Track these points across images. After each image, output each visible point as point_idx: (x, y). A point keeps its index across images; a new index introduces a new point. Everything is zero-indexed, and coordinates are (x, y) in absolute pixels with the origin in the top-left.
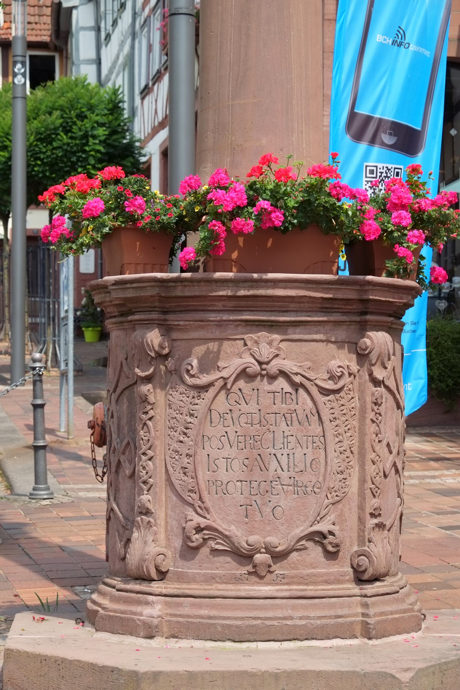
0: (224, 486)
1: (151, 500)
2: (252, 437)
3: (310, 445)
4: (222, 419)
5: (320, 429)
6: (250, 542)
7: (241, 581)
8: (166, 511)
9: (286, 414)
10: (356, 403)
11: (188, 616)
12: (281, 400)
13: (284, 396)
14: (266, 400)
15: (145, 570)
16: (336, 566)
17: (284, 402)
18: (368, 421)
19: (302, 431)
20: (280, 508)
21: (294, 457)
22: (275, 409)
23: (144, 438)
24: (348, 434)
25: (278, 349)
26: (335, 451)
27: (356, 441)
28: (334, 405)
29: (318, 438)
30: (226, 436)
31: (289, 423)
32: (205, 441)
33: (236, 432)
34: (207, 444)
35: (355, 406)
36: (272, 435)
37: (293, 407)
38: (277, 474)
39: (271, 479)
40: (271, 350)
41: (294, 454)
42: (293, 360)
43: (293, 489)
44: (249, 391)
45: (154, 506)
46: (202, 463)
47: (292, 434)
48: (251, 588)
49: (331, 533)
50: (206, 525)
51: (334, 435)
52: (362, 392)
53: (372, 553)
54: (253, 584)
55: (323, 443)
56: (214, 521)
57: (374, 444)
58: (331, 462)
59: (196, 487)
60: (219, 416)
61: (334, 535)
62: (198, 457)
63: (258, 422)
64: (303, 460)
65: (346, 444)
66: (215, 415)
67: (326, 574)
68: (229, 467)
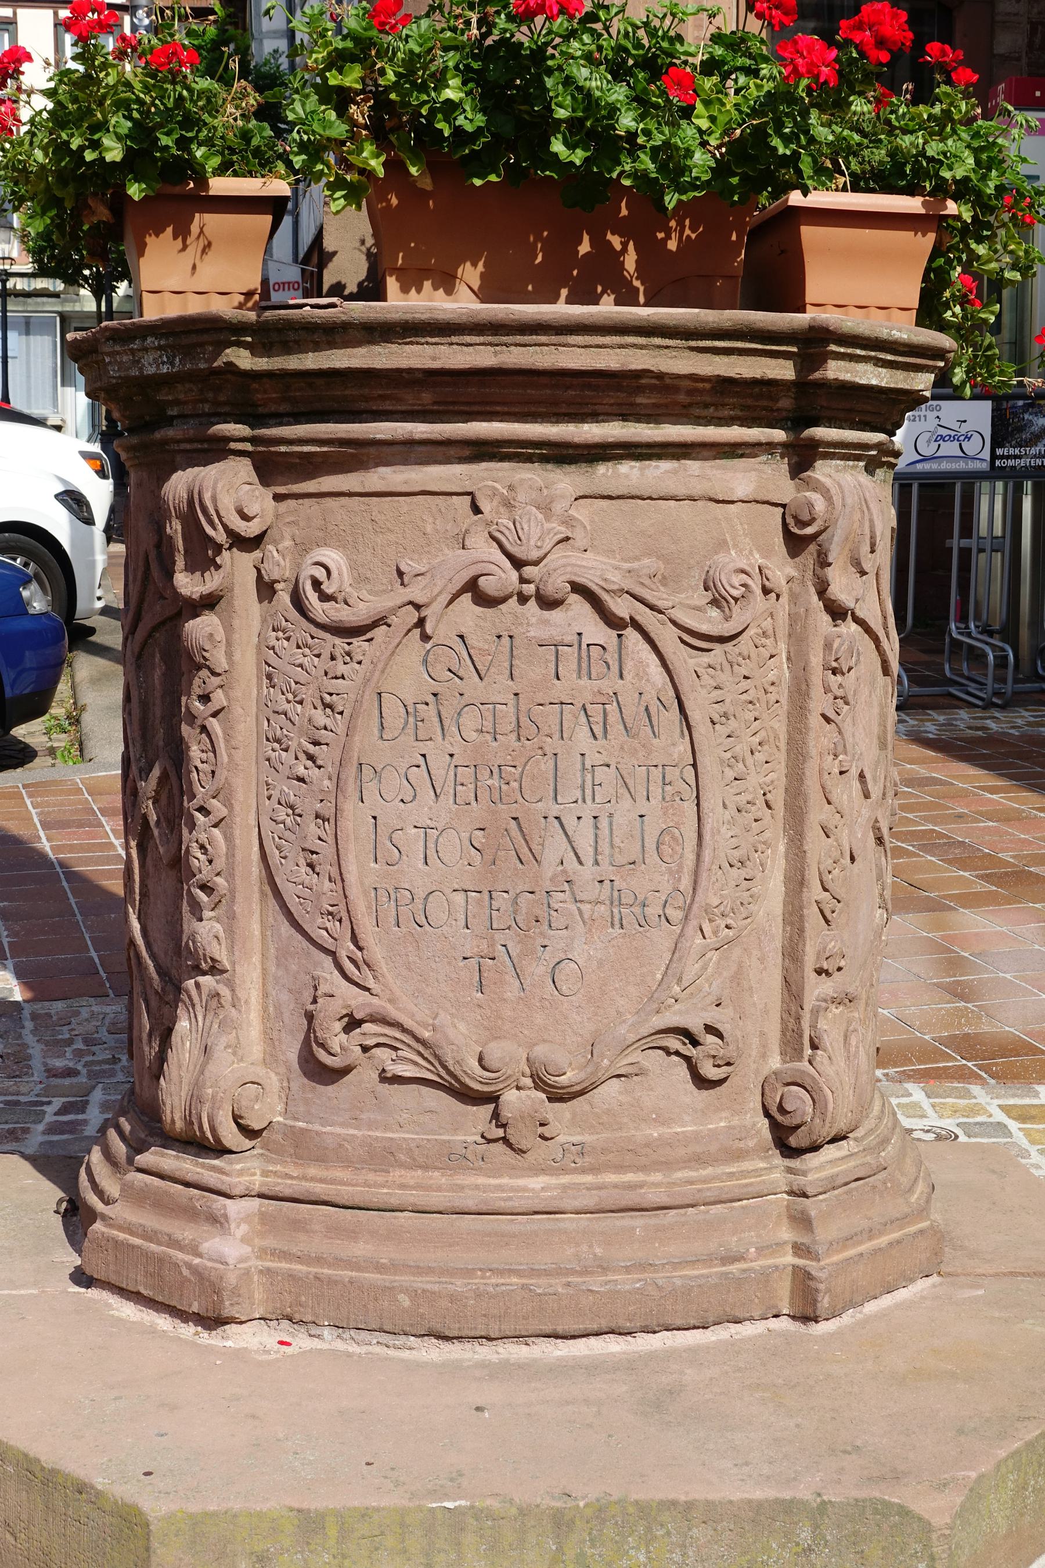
0: (419, 903)
1: (222, 935)
2: (496, 770)
3: (656, 791)
4: (411, 720)
5: (684, 746)
6: (491, 1061)
7: (464, 1162)
8: (263, 963)
9: (589, 707)
10: (780, 670)
11: (319, 1260)
12: (575, 666)
13: (584, 654)
14: (534, 669)
15: (206, 1126)
16: (724, 1114)
17: (584, 672)
18: (815, 721)
19: (634, 752)
20: (572, 965)
21: (611, 824)
22: (559, 690)
23: (200, 766)
24: (760, 757)
25: (568, 521)
26: (725, 806)
27: (778, 775)
28: (724, 677)
29: (677, 771)
30: (423, 767)
31: (598, 730)
32: (365, 778)
33: (451, 755)
34: (371, 789)
35: (779, 678)
36: (551, 763)
37: (608, 685)
38: (564, 871)
39: (548, 885)
40: (547, 526)
41: (611, 815)
42: (610, 552)
43: (609, 913)
44: (486, 641)
45: (231, 950)
46: (356, 838)
47: (607, 760)
48: (493, 1181)
49: (710, 1029)
50: (368, 1011)
51: (722, 761)
52: (798, 637)
53: (821, 1081)
54: (496, 1173)
55: (693, 783)
56: (390, 1001)
57: (829, 784)
58: (713, 835)
59: (342, 906)
60: (403, 710)
61: (720, 1035)
62: (347, 824)
63: (510, 728)
64: (637, 833)
65: (754, 780)
66: (393, 709)
67: (696, 1137)
68: (431, 853)
